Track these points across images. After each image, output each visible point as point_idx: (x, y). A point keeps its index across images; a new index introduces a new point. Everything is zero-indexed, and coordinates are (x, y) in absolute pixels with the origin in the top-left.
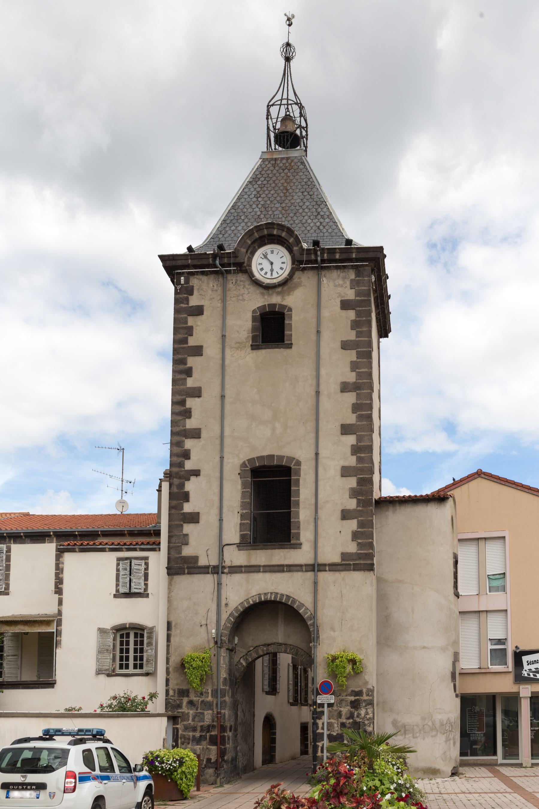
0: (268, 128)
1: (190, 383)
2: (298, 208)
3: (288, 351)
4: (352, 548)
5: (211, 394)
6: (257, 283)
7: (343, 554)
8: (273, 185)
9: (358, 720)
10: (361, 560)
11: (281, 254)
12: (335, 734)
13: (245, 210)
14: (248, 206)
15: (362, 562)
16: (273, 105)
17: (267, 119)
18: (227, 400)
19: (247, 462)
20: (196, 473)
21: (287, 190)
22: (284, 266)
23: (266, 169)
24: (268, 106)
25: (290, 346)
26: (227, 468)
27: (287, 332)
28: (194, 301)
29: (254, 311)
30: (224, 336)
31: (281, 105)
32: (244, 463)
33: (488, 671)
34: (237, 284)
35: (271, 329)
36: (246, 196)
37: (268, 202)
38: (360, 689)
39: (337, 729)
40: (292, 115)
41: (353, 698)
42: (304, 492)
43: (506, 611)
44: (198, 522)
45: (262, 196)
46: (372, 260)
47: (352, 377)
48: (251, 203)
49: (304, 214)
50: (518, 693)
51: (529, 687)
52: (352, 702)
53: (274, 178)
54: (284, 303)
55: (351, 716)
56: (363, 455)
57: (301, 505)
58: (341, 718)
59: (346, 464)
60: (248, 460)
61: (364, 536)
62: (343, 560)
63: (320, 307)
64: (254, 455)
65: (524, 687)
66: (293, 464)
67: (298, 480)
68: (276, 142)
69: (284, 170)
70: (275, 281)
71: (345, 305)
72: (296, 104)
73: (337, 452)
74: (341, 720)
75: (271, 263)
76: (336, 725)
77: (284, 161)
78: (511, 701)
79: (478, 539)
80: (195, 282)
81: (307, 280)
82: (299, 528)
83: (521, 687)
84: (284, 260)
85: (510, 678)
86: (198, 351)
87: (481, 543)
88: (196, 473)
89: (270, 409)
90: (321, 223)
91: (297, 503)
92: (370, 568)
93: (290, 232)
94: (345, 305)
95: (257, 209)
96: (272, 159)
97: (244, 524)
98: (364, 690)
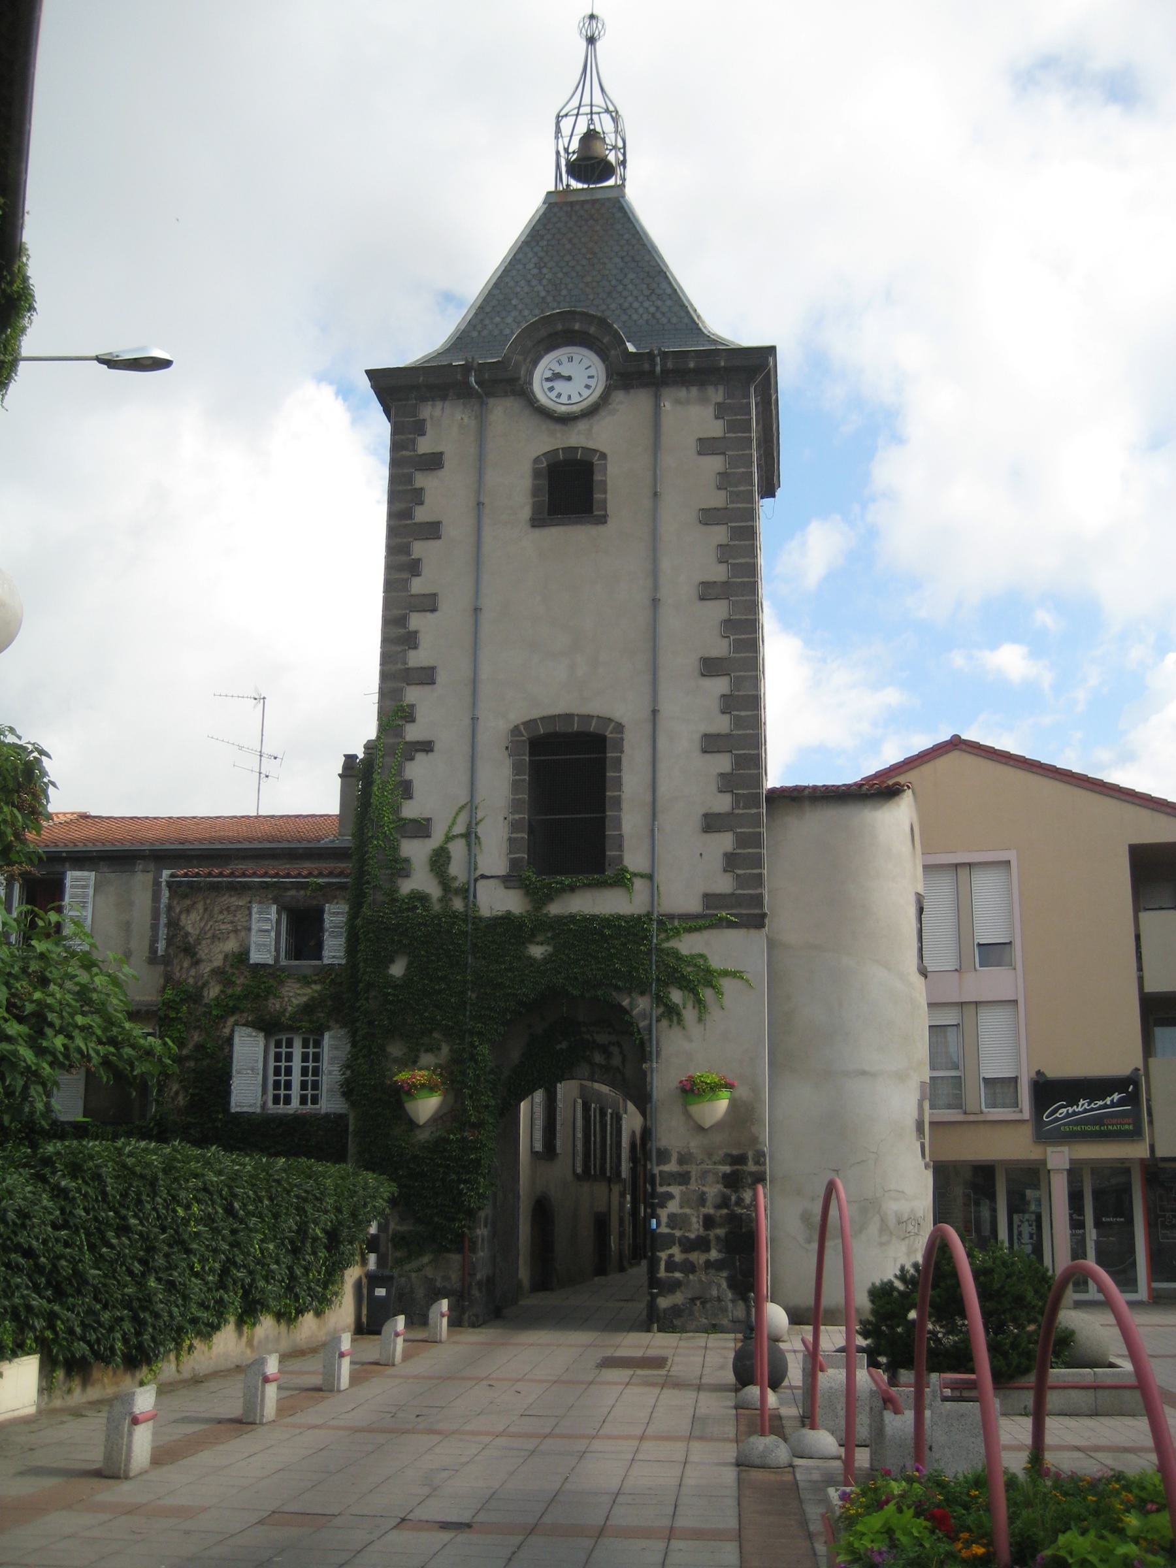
0: (558, 153)
1: (418, 586)
2: (614, 282)
3: (601, 528)
4: (724, 884)
5: (453, 608)
6: (545, 414)
7: (706, 896)
8: (568, 246)
9: (739, 1211)
10: (742, 909)
11: (586, 363)
12: (692, 1236)
13: (518, 289)
14: (523, 283)
15: (744, 912)
16: (566, 115)
17: (557, 138)
18: (487, 616)
19: (522, 728)
20: (426, 747)
21: (594, 254)
22: (592, 382)
23: (555, 220)
24: (558, 116)
25: (603, 520)
26: (483, 738)
27: (597, 496)
28: (424, 446)
29: (537, 460)
30: (480, 504)
31: (577, 115)
32: (516, 727)
33: (980, 1118)
34: (502, 414)
35: (569, 490)
36: (520, 267)
37: (560, 275)
38: (741, 1152)
39: (696, 1226)
40: (599, 129)
41: (727, 1169)
42: (631, 781)
43: (1015, 1002)
44: (429, 837)
45: (549, 265)
46: (752, 369)
47: (719, 573)
48: (529, 277)
49: (625, 293)
50: (1044, 1162)
51: (1065, 1149)
52: (725, 1176)
53: (570, 235)
54: (591, 445)
55: (724, 1203)
56: (743, 713)
57: (625, 805)
58: (704, 1206)
59: (713, 729)
60: (524, 724)
61: (745, 861)
62: (707, 906)
63: (658, 450)
64: (536, 714)
65: (1055, 1149)
66: (610, 729)
67: (619, 760)
68: (569, 172)
69: (587, 221)
70: (575, 408)
71: (706, 446)
72: (607, 111)
73: (692, 708)
74: (704, 1210)
75: (569, 378)
76: (694, 1220)
77: (587, 207)
78: (1030, 1176)
79: (957, 866)
80: (427, 411)
81: (631, 409)
82: (620, 847)
83: (1049, 1149)
84: (592, 372)
85: (1027, 1131)
86: (432, 530)
87: (963, 873)
88: (426, 747)
89: (564, 634)
90: (658, 308)
91: (618, 802)
92: (757, 921)
93: (603, 323)
94: (706, 446)
95: (540, 288)
96: (566, 203)
97: (516, 839)
98: (750, 1154)
